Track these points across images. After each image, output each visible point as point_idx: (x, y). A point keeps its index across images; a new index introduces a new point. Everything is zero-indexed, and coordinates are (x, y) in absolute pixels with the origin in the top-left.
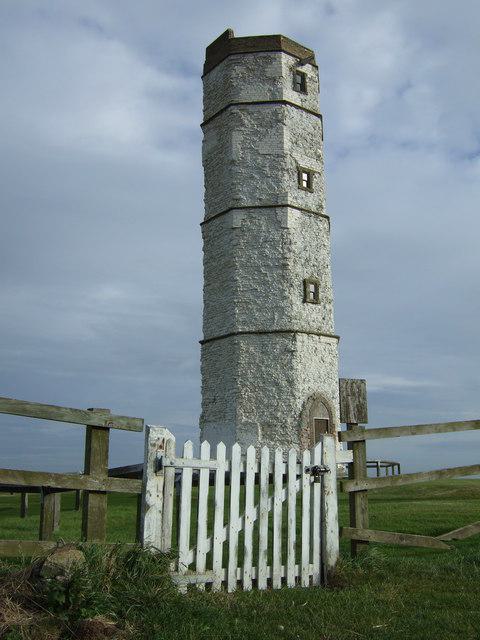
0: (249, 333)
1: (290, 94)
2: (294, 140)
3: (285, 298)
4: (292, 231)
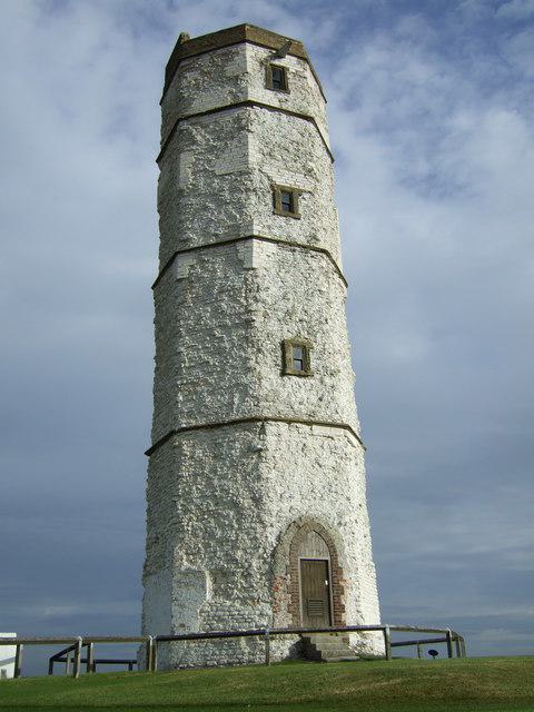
4: (261, 272)
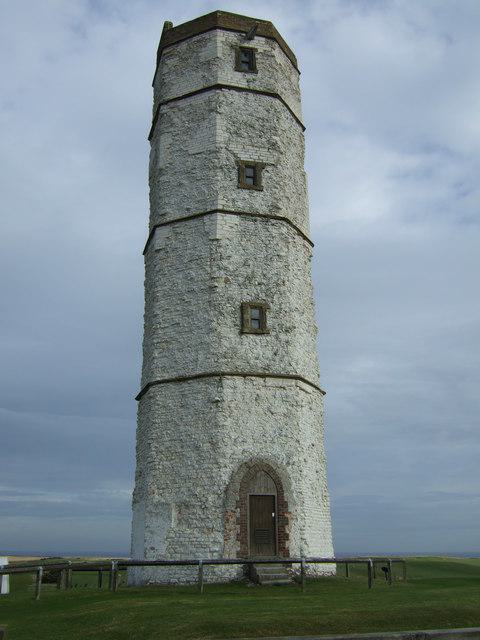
0: (168, 381)
1: (228, 75)
2: (233, 129)
3: (212, 330)
4: (223, 243)
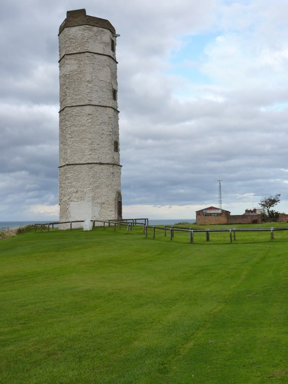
0: (97, 163)
